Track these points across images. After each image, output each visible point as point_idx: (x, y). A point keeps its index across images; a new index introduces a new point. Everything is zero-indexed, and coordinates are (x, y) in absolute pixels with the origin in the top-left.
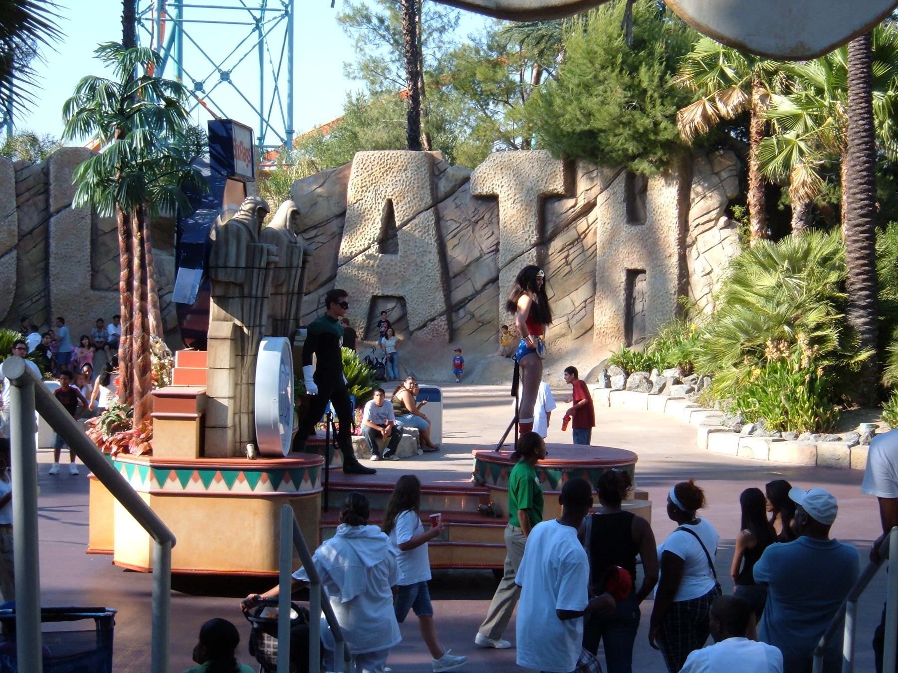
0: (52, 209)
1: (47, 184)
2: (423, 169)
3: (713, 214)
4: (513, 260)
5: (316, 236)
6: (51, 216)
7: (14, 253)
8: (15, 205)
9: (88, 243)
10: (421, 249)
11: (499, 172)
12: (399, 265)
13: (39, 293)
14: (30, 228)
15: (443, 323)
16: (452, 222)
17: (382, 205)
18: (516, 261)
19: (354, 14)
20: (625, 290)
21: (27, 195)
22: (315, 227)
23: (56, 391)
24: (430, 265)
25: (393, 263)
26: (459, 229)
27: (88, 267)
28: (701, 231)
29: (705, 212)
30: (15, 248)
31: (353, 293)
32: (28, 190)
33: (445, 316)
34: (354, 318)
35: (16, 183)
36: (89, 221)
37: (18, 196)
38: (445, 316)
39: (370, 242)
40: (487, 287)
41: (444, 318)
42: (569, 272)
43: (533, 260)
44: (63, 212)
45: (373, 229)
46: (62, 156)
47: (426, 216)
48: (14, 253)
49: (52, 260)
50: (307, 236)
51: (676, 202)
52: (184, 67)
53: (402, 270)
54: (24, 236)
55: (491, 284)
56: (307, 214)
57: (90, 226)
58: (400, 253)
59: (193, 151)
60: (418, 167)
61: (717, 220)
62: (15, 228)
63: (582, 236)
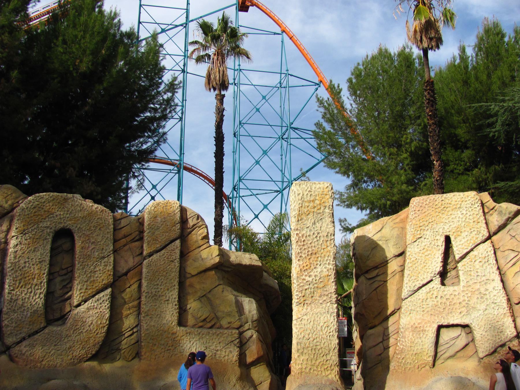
0: (145, 253)
1: (142, 232)
5: (377, 276)
7: (109, 290)
10: (484, 278)
12: (462, 294)
13: (133, 329)
14: (125, 270)
16: (510, 251)
17: (443, 239)
21: (124, 241)
22: (376, 268)
23: (357, 73)
24: (495, 293)
25: (457, 293)
27: (176, 305)
30: (111, 287)
31: (419, 324)
32: (125, 237)
34: (421, 347)
36: (177, 265)
39: (432, 275)
44: (155, 256)
45: (434, 263)
47: (485, 248)
48: (109, 290)
49: (143, 299)
50: (369, 276)
53: (466, 298)
54: (120, 277)
56: (368, 256)
57: (178, 269)
58: (462, 284)
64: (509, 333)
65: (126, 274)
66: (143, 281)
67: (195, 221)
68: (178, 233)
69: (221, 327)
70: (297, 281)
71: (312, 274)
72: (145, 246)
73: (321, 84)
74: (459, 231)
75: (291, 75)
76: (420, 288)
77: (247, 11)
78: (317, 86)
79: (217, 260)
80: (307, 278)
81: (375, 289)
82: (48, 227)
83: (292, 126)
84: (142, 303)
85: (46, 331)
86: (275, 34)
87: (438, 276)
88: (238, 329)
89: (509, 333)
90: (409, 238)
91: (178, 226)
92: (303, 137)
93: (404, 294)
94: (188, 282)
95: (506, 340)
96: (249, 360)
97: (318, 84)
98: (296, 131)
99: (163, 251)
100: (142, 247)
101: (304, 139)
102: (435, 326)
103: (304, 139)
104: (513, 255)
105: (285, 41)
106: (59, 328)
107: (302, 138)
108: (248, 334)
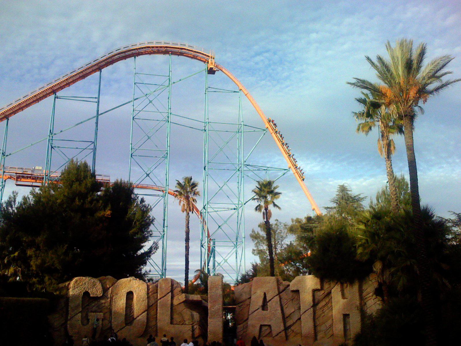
0: (159, 298)
3: (371, 294)
5: (242, 305)
7: (146, 312)
17: (263, 294)
22: (241, 302)
48: (146, 312)
58: (269, 310)
65: (152, 306)
66: (158, 308)
67: (176, 285)
69: (186, 324)
72: (159, 295)
74: (268, 291)
76: (255, 311)
77: (214, 74)
79: (184, 299)
80: (213, 310)
81: (241, 310)
82: (124, 291)
84: (158, 316)
85: (126, 328)
88: (191, 325)
90: (252, 293)
91: (170, 287)
93: (250, 313)
94: (174, 308)
96: (196, 336)
99: (165, 297)
100: (157, 295)
102: (269, 324)
104: (286, 301)
106: (130, 327)
108: (195, 327)
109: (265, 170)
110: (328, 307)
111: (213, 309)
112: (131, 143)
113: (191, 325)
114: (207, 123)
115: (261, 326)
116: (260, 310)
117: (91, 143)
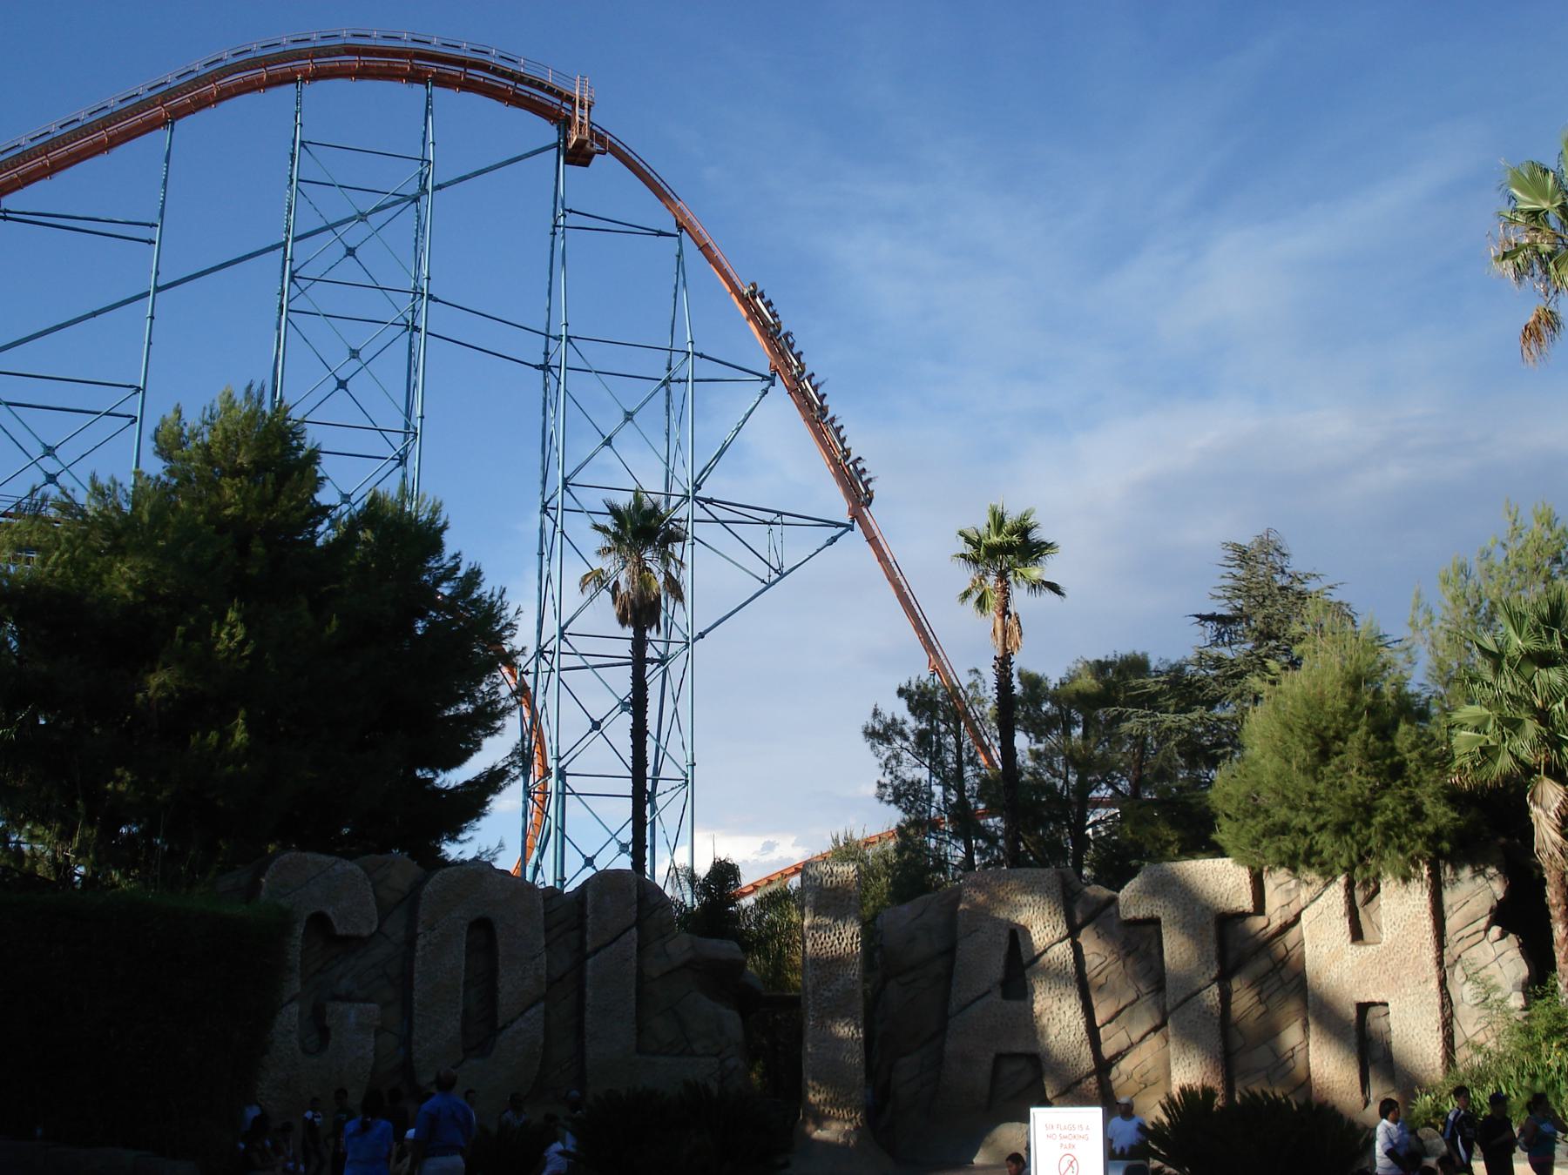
0: (589, 948)
1: (582, 916)
2: (1054, 891)
3: (1483, 923)
4: (1185, 1000)
6: (587, 957)
7: (542, 1005)
8: (543, 942)
9: (633, 991)
11: (1160, 889)
15: (1093, 1087)
17: (1006, 934)
18: (1191, 1001)
19: (885, 729)
20: (1356, 1030)
26: (1104, 965)
28: (1466, 946)
29: (1472, 921)
33: (1095, 1077)
35: (545, 914)
37: (547, 930)
38: (1095, 1077)
40: (1148, 1037)
41: (1093, 1079)
42: (1264, 1013)
43: (1215, 999)
46: (601, 880)
49: (588, 1015)
51: (1428, 911)
52: (566, 833)
55: (1152, 1034)
59: (1183, 735)
60: (1049, 888)
61: (1487, 930)
62: (543, 972)
63: (1279, 966)
64: (1086, 1067)
68: (634, 919)
70: (813, 997)
71: (832, 987)
73: (778, 378)
75: (701, 356)
77: (586, 165)
78: (766, 384)
80: (827, 994)
83: (698, 494)
86: (660, 233)
87: (998, 986)
89: (1086, 1067)
91: (635, 907)
92: (720, 519)
95: (1082, 1076)
97: (768, 379)
98: (708, 506)
99: (614, 945)
101: (723, 523)
103: (723, 523)
105: (686, 257)
107: (717, 521)
109: (765, 523)
110: (1281, 978)
111: (830, 991)
112: (564, 322)
113: (717, 1055)
114: (564, 338)
115: (999, 1058)
116: (997, 995)
117: (132, 391)
